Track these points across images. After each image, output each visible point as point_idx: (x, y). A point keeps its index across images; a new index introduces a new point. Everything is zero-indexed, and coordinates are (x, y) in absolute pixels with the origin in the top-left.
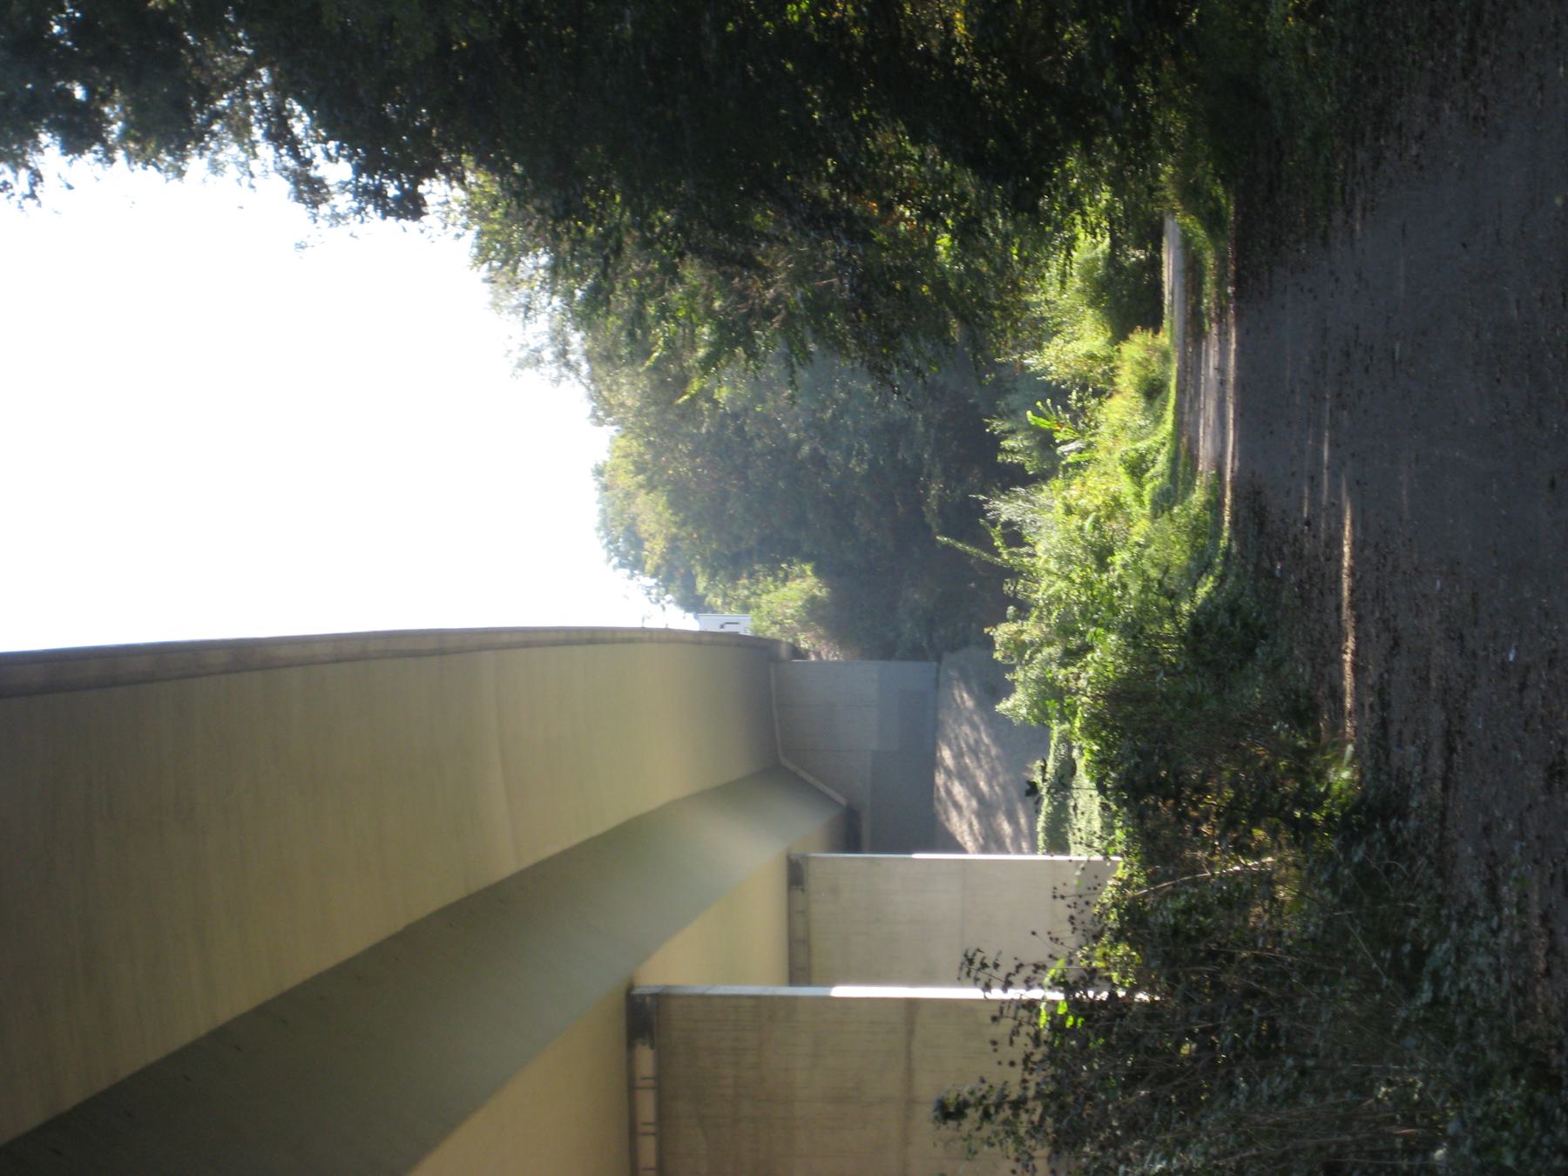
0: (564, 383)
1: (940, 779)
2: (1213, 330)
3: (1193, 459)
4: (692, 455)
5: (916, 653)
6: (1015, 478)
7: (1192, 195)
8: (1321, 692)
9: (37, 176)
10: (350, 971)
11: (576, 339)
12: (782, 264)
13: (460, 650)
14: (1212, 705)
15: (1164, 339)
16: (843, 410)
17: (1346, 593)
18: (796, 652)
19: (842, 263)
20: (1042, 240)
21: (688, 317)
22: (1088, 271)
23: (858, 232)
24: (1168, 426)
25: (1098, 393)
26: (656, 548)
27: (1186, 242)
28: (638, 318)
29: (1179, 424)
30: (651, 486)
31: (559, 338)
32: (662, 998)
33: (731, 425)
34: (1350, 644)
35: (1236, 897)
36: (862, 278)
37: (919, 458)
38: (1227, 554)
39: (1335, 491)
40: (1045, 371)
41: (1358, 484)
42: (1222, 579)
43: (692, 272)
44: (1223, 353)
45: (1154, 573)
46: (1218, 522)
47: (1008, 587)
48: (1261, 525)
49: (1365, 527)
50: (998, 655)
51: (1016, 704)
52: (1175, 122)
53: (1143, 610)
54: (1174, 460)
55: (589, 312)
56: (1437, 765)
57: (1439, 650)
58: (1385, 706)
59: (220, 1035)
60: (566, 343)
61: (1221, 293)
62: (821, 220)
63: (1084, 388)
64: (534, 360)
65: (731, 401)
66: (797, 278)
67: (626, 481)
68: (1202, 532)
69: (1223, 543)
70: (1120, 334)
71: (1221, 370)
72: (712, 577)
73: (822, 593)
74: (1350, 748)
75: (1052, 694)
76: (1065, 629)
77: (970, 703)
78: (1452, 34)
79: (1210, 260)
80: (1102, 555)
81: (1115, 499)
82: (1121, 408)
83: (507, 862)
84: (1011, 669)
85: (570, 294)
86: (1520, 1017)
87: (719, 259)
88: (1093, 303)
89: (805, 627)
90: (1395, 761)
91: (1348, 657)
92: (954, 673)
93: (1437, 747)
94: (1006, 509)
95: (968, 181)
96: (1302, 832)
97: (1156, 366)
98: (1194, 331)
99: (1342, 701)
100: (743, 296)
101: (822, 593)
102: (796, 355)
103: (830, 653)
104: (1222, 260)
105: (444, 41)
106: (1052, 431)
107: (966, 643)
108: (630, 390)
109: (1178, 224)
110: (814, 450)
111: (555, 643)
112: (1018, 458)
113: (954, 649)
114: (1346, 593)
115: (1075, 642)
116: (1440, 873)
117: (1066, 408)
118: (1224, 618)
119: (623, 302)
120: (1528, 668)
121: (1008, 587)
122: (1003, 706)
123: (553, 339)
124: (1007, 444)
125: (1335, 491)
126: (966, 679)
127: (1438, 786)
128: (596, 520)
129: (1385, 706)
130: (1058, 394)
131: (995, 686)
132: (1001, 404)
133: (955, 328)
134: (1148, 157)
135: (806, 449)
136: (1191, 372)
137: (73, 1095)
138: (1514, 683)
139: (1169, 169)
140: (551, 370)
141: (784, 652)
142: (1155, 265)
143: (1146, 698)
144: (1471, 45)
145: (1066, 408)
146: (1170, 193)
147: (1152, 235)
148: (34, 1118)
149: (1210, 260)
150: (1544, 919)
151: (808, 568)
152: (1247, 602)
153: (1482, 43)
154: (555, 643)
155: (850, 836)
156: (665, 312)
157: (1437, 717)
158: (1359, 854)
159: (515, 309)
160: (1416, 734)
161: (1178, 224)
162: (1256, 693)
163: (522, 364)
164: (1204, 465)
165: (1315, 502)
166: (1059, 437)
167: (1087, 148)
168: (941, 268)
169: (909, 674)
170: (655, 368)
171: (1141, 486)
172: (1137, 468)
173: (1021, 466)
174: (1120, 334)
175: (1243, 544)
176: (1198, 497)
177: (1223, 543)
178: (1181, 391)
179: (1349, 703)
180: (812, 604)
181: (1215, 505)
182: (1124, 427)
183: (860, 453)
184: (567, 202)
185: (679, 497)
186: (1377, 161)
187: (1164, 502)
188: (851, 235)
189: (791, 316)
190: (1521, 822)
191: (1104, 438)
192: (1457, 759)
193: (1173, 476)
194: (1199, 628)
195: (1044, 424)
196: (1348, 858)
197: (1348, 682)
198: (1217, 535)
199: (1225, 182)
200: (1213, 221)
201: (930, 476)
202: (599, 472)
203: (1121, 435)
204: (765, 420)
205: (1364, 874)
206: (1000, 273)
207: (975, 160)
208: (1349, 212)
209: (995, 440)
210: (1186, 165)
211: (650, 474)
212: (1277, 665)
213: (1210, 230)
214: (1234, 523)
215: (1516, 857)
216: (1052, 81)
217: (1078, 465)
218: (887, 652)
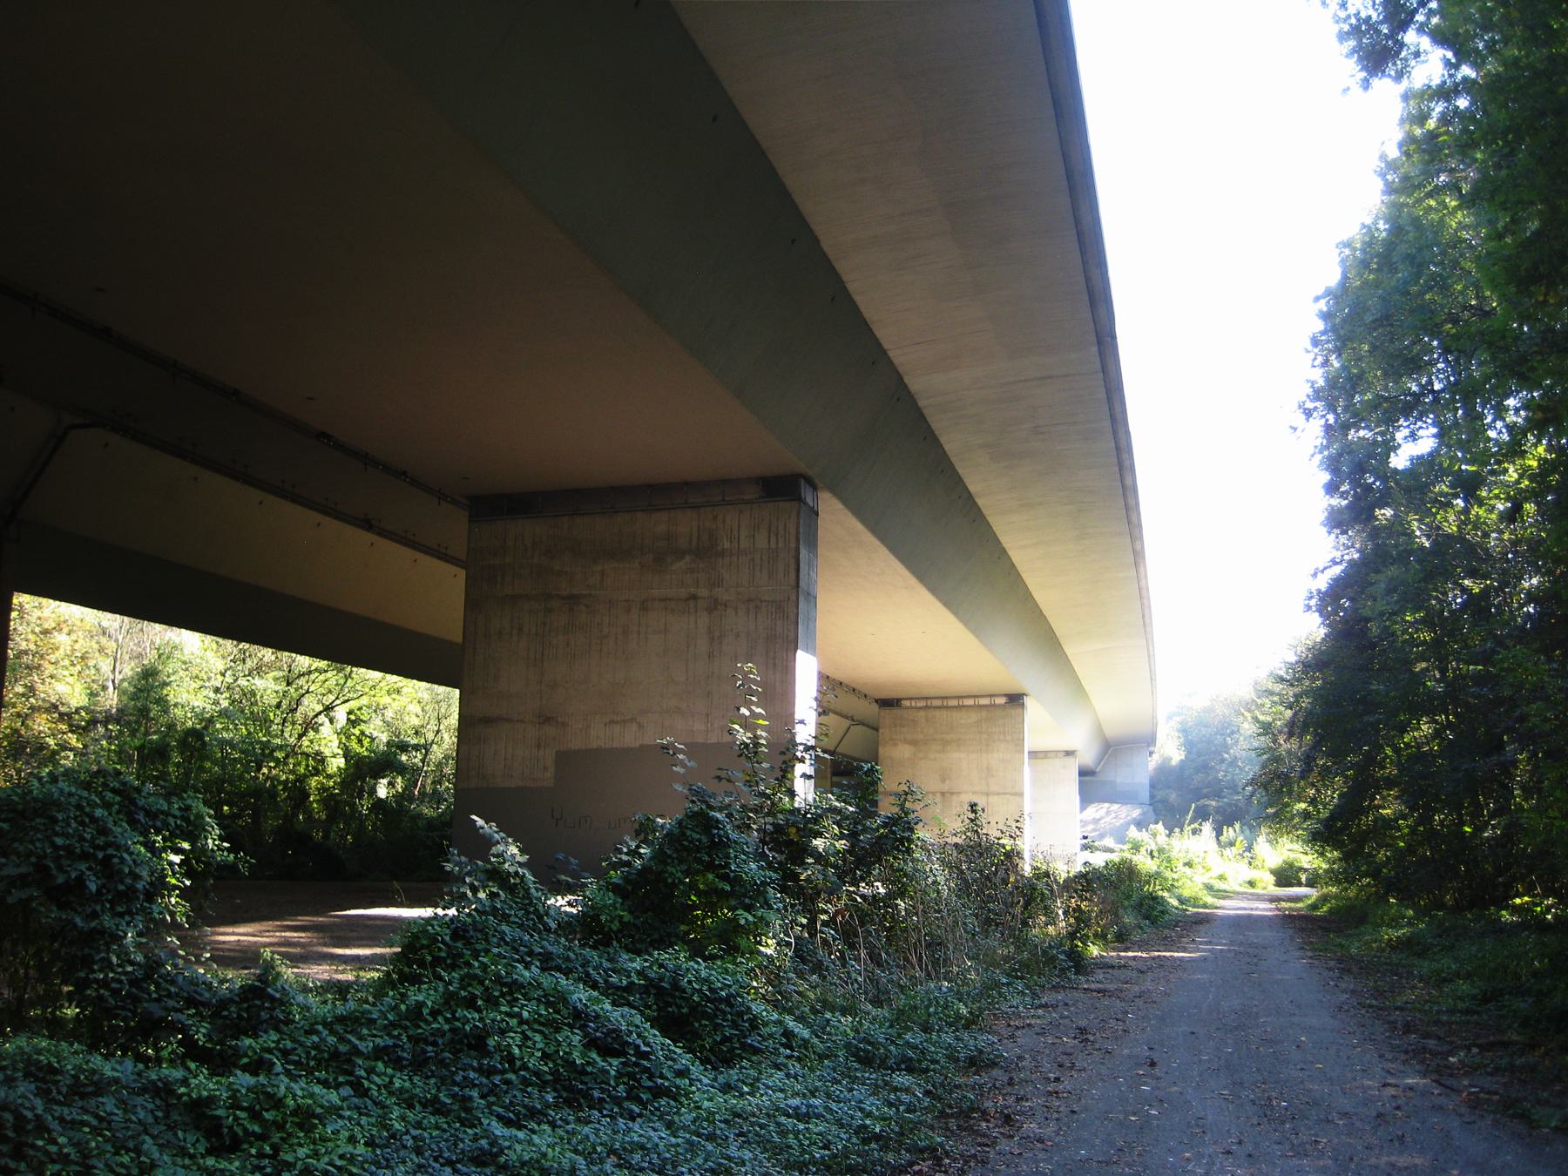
1: (1107, 805)
2: (1273, 906)
3: (1224, 898)
5: (1152, 797)
6: (1219, 832)
7: (1324, 899)
8: (1129, 945)
10: (1028, 596)
12: (1293, 745)
14: (1126, 903)
16: (1241, 769)
17: (1164, 954)
18: (1151, 753)
19: (1293, 768)
20: (1306, 842)
23: (1304, 775)
25: (1250, 863)
27: (1307, 897)
28: (1271, 693)
33: (1236, 729)
34: (1144, 955)
35: (1048, 911)
36: (1286, 775)
37: (1224, 797)
38: (1186, 910)
39: (1204, 950)
41: (1205, 959)
42: (1177, 908)
43: (1289, 713)
44: (1264, 910)
45: (1180, 883)
46: (1198, 907)
47: (1177, 830)
48: (1196, 923)
49: (1189, 961)
51: (1133, 833)
52: (1352, 892)
53: (1166, 879)
56: (1093, 986)
57: (1136, 988)
58: (1119, 968)
59: (1004, 551)
61: (1286, 909)
62: (1308, 760)
63: (1252, 858)
66: (1289, 752)
68: (1194, 901)
69: (1190, 909)
70: (1273, 872)
71: (1257, 909)
74: (1105, 954)
75: (1136, 848)
76: (1161, 851)
77: (1134, 816)
78: (1376, 999)
79: (1300, 905)
80: (1189, 864)
83: (1070, 650)
85: (1281, 669)
86: (995, 1015)
87: (1291, 724)
90: (1100, 971)
91: (1140, 954)
93: (1100, 986)
94: (1207, 828)
95: (1325, 814)
96: (1072, 936)
98: (1274, 899)
99: (1124, 951)
100: (1280, 732)
101: (1174, 763)
102: (1260, 751)
104: (1298, 910)
105: (1368, 620)
107: (1157, 814)
109: (1314, 893)
113: (1154, 811)
114: (1164, 954)
115: (1156, 854)
116: (1053, 987)
118: (1160, 908)
119: (1278, 688)
120: (1124, 1022)
121: (1177, 830)
122: (1133, 827)
125: (1204, 950)
126: (1143, 814)
127: (1086, 986)
129: (1119, 968)
130: (1249, 848)
131: (1140, 824)
132: (1245, 827)
133: (1271, 811)
134: (1338, 882)
135: (1226, 756)
136: (1259, 898)
137: (980, 502)
138: (1120, 1016)
139: (1334, 890)
141: (1151, 749)
142: (1300, 884)
143: (1130, 879)
144: (1371, 1006)
146: (1325, 890)
147: (1311, 884)
148: (972, 488)
149: (1300, 905)
150: (1029, 1025)
151: (1183, 757)
152: (1167, 917)
153: (1370, 1010)
155: (1084, 773)
157: (1111, 987)
158: (1062, 957)
160: (1107, 979)
161: (1314, 893)
162: (1129, 919)
165: (1201, 943)
167: (1340, 859)
169: (1145, 795)
170: (1253, 700)
172: (1221, 878)
174: (1273, 872)
175: (1189, 916)
176: (1210, 900)
177: (1190, 909)
178: (1251, 894)
179: (1122, 954)
181: (1205, 906)
184: (1309, 666)
186: (1330, 969)
187: (1209, 888)
190: (1067, 1017)
192: (1095, 994)
193: (1219, 891)
194: (1154, 898)
196: (1061, 953)
197: (1130, 954)
198: (1194, 907)
200: (1314, 907)
205: (1053, 959)
206: (1294, 827)
207: (1333, 817)
208: (1311, 958)
209: (1231, 825)
210: (1336, 897)
212: (1141, 928)
213: (1310, 905)
214: (1198, 913)
215: (1054, 1015)
216: (123, 842)
218: (1152, 786)
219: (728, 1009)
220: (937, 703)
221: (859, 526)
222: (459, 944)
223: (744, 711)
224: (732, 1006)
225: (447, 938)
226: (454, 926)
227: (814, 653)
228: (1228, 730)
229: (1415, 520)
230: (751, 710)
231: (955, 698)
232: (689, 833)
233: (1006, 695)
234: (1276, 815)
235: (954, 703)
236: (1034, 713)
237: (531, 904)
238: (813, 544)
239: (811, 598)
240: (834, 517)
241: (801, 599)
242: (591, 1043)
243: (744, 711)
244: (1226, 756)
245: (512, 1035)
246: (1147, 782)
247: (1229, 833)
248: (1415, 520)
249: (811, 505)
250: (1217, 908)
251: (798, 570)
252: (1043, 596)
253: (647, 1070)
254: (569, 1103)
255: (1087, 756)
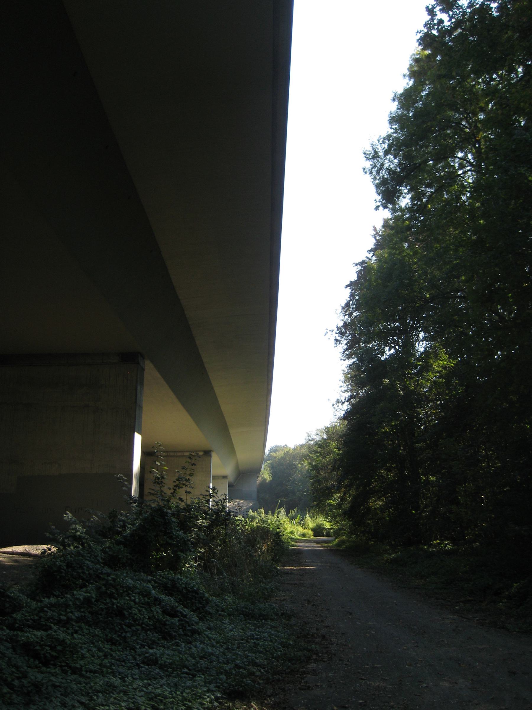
0: (305, 441)
1: (238, 500)
3: (296, 542)
4: (290, 461)
5: (258, 496)
6: (287, 513)
9: (345, 360)
10: (219, 407)
11: (312, 442)
13: (265, 424)
15: (312, 537)
18: (258, 477)
21: (317, 460)
22: (322, 524)
24: (299, 538)
26: (274, 454)
28: (317, 452)
29: (299, 539)
30: (285, 454)
31: (313, 440)
32: (211, 456)
40: (306, 518)
50: (259, 510)
51: (251, 513)
54: (294, 539)
55: (317, 444)
60: (312, 441)
64: (309, 436)
65: (298, 467)
67: (285, 450)
70: (313, 530)
72: (270, 464)
73: (267, 481)
79: (330, 545)
81: (286, 529)
82: (301, 530)
83: (232, 431)
84: (257, 512)
88: (317, 525)
89: (262, 478)
92: (255, 502)
97: (307, 536)
101: (267, 481)
103: (258, 482)
106: (297, 518)
108: (304, 451)
110: (291, 480)
111: (264, 439)
112: (291, 513)
117: (300, 521)
122: (251, 511)
123: (312, 439)
124: (293, 511)
128: (278, 445)
133: (315, 503)
135: (291, 479)
140: (307, 438)
141: (258, 475)
142: (323, 536)
145: (300, 521)
147: (328, 535)
149: (330, 545)
151: (271, 479)
154: (264, 439)
155: (230, 486)
156: (318, 457)
159: (317, 433)
163: (308, 434)
164: (296, 544)
166: (296, 520)
168: (326, 501)
171: (289, 533)
172: (292, 533)
173: (289, 513)
174: (313, 530)
180: (265, 480)
182: (298, 530)
183: (290, 487)
185: (283, 458)
188: (338, 487)
189: (318, 476)
191: (296, 527)
195: (298, 517)
199: (346, 547)
201: (287, 499)
202: (286, 445)
203: (296, 530)
204: (295, 472)
209: (293, 509)
211: (287, 453)
217: (291, 523)
218: (258, 492)
219: (197, 596)
220: (172, 454)
221: (159, 375)
222: (70, 570)
223: (157, 463)
224: (198, 594)
225: (65, 567)
226: (66, 562)
227: (140, 434)
228: (291, 467)
229: (398, 384)
230: (160, 463)
231: (173, 452)
232: (156, 518)
233: (203, 451)
234: (317, 505)
235: (180, 454)
236: (215, 459)
237: (92, 551)
238: (142, 384)
239: (141, 407)
240: (149, 368)
241: (137, 408)
242: (165, 612)
243: (157, 463)
244: (291, 479)
245: (134, 609)
246: (256, 490)
247: (292, 513)
248: (398, 384)
249: (142, 366)
250: (299, 546)
251: (136, 396)
252: (225, 408)
253: (187, 622)
254: (164, 638)
255: (231, 478)
